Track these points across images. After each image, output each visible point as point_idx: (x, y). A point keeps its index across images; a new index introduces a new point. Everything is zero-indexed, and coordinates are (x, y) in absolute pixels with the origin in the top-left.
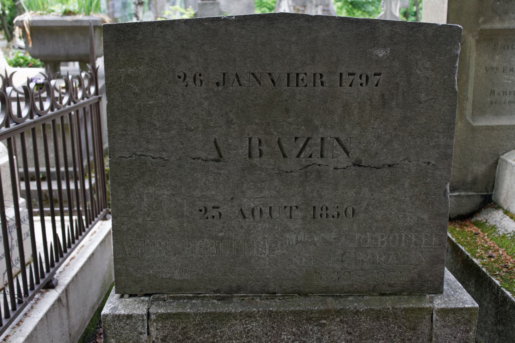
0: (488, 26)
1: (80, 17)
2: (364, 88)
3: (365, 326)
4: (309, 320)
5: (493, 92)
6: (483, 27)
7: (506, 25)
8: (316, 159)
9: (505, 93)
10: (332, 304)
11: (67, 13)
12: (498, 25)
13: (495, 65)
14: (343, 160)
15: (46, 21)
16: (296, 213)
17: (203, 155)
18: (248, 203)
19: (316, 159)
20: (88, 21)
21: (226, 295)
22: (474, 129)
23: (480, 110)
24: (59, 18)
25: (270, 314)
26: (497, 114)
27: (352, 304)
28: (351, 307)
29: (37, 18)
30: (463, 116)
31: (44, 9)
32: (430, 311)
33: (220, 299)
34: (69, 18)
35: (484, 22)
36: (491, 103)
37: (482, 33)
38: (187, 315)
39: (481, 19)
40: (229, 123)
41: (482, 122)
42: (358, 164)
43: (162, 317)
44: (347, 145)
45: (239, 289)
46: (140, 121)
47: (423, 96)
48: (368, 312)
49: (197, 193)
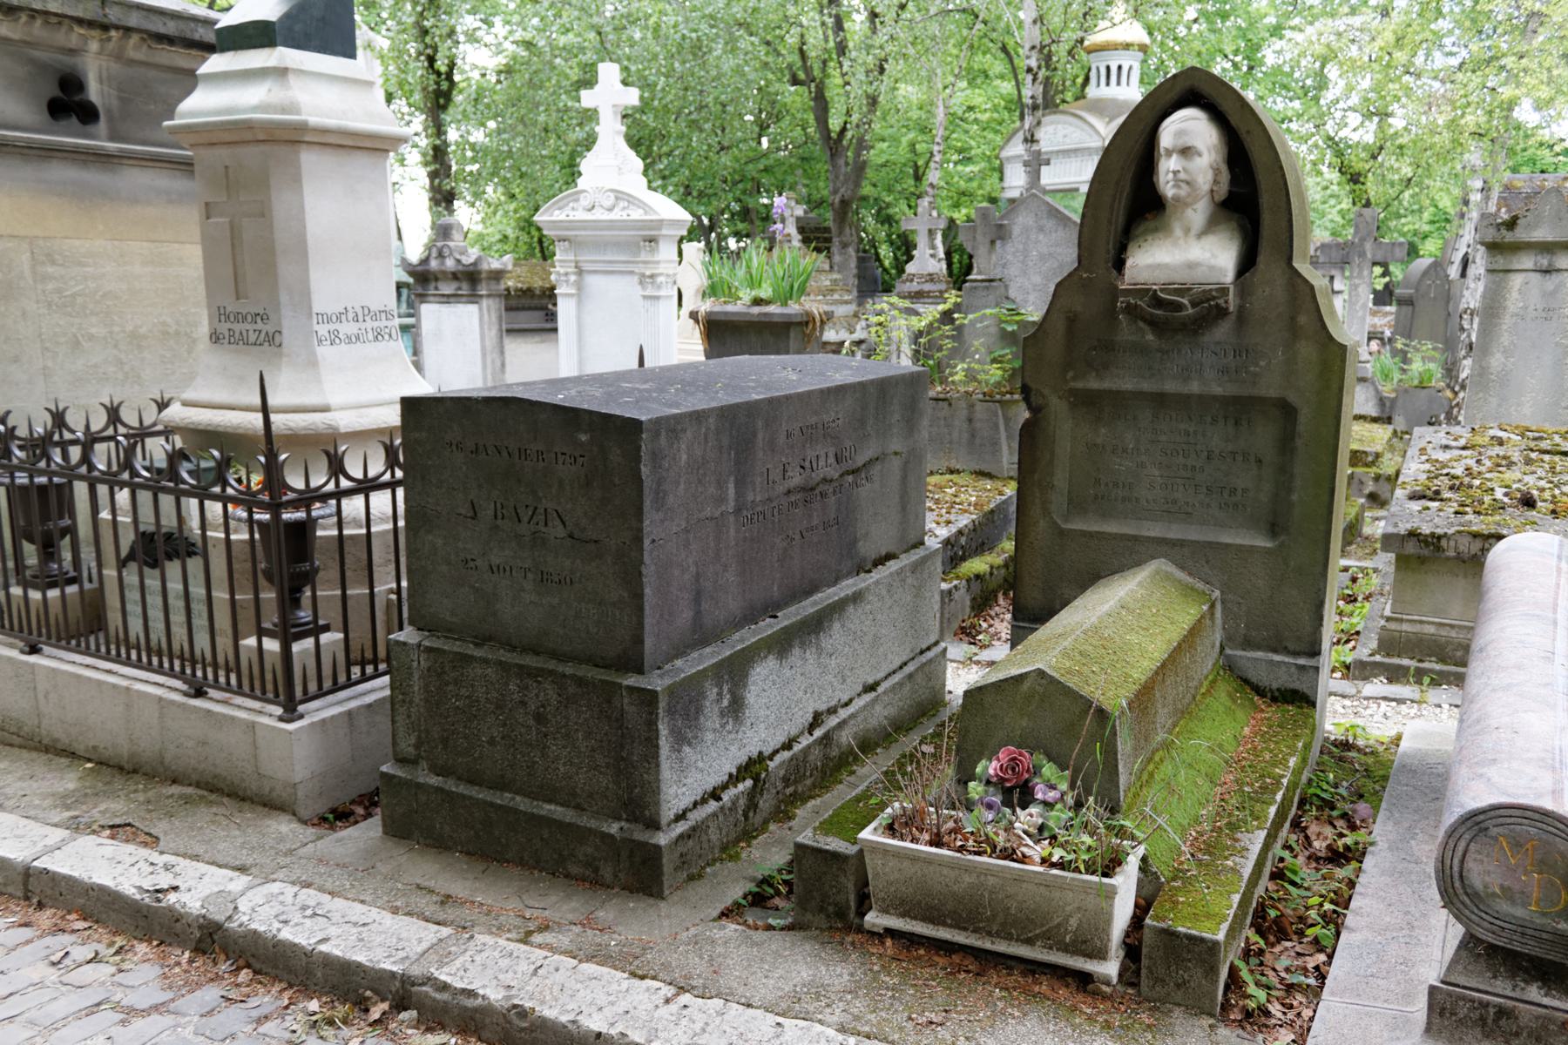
0: (1080, 385)
1: (772, 309)
2: (573, 468)
3: (571, 690)
4: (529, 675)
5: (1097, 481)
6: (1072, 384)
7: (1106, 385)
8: (541, 527)
9: (1116, 485)
10: (552, 665)
11: (757, 302)
12: (1093, 384)
13: (1099, 441)
14: (560, 532)
15: (726, 313)
16: (530, 575)
17: (463, 511)
18: (496, 561)
19: (541, 527)
20: (782, 315)
21: (480, 641)
22: (1062, 533)
23: (1077, 505)
24: (744, 310)
25: (501, 663)
26: (1104, 516)
27: (568, 669)
28: (560, 669)
29: (717, 309)
30: (1046, 512)
31: (730, 295)
32: (620, 685)
33: (476, 645)
34: (756, 310)
35: (1074, 379)
36: (1096, 497)
37: (1073, 392)
38: (444, 651)
39: (1070, 374)
40: (480, 486)
41: (1078, 525)
42: (571, 536)
43: (429, 650)
44: (566, 519)
45: (490, 639)
46: (423, 478)
47: (617, 481)
48: (573, 676)
49: (460, 545)
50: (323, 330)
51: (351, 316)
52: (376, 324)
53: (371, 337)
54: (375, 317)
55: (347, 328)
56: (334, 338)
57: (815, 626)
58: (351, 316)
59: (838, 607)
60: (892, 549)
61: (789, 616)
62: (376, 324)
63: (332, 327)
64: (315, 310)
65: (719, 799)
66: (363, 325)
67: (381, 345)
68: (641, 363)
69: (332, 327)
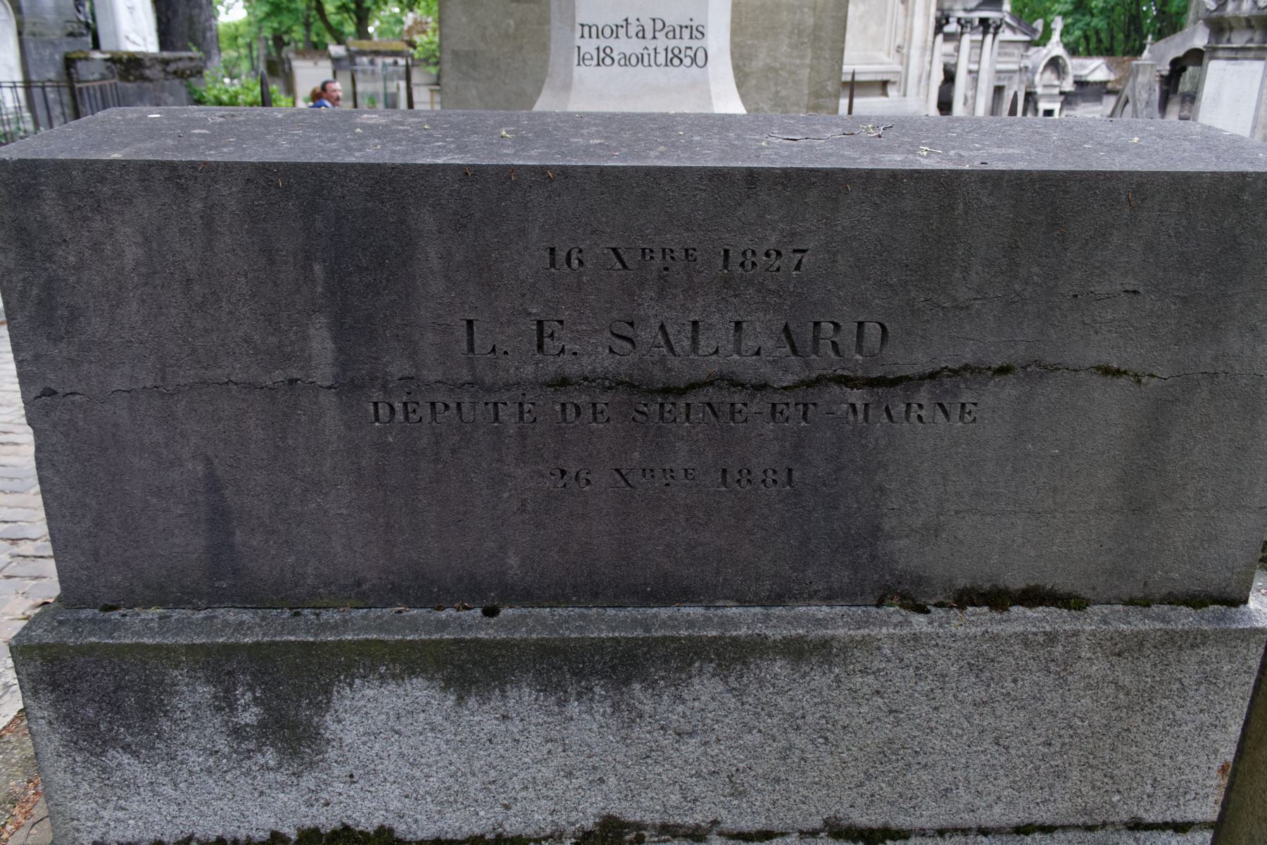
50: (589, 46)
51: (633, 30)
52: (672, 43)
53: (661, 59)
54: (673, 33)
55: (624, 46)
56: (603, 58)
57: (623, 666)
58: (633, 30)
59: (685, 655)
60: (1098, 381)
61: (607, 623)
62: (672, 43)
63: (602, 43)
64: (579, 20)
65: (647, 630)
66: (652, 45)
67: (674, 72)
68: (945, 105)
69: (602, 43)
